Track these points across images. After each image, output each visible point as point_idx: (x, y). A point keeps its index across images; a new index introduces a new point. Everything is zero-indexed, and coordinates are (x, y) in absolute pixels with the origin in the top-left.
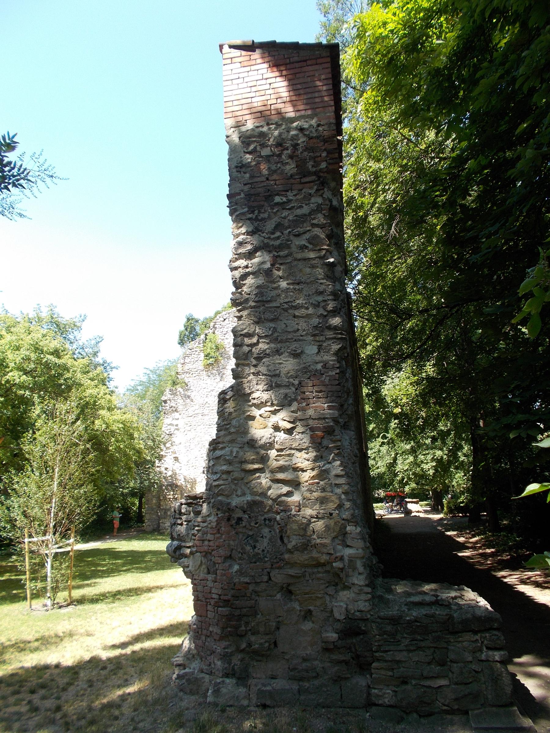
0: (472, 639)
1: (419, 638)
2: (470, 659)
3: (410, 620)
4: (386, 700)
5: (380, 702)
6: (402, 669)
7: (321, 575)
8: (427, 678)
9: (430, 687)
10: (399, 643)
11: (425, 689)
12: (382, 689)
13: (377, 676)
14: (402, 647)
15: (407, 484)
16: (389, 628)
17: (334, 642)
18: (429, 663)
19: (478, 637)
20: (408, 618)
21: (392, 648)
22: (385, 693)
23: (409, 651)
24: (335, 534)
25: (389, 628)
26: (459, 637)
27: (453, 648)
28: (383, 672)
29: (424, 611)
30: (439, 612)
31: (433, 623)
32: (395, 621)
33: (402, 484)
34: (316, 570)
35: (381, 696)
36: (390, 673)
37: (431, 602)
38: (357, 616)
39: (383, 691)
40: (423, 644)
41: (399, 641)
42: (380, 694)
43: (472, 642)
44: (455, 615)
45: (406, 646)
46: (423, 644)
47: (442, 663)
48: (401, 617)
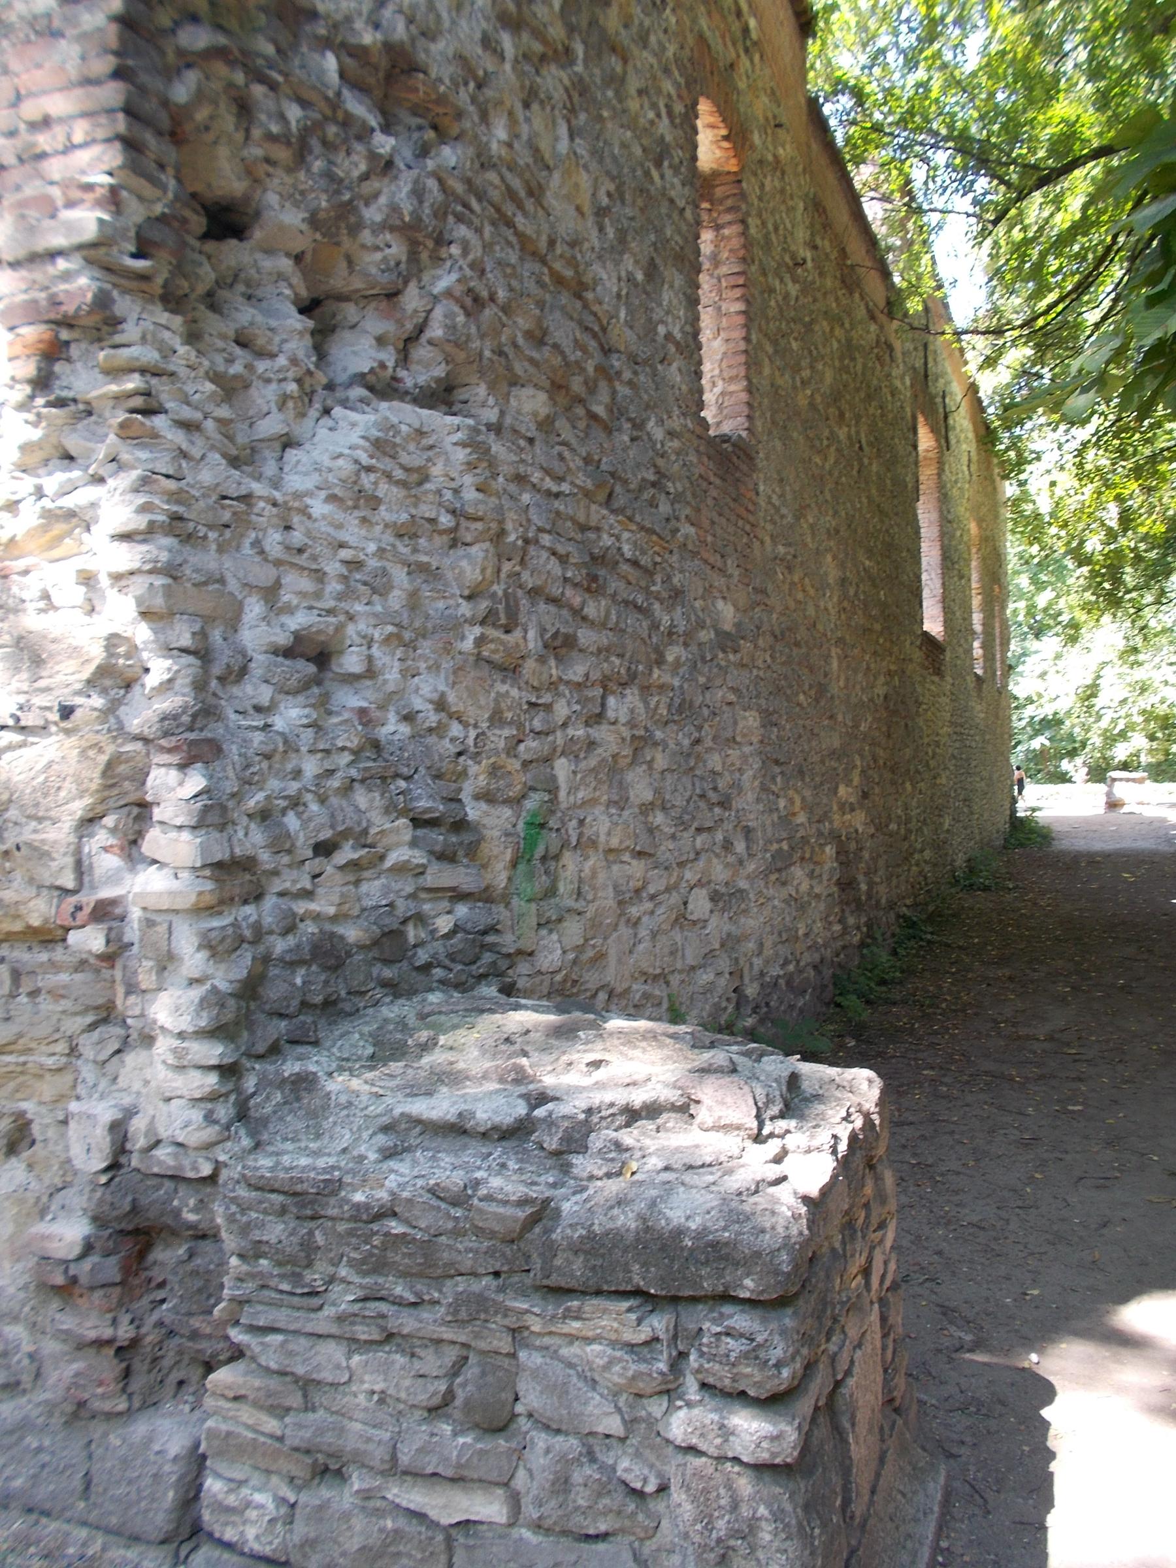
0: (629, 1336)
1: (398, 1290)
2: (614, 1425)
3: (367, 1206)
4: (251, 1532)
5: (229, 1535)
6: (321, 1413)
7: (64, 977)
8: (414, 1474)
9: (419, 1516)
10: (315, 1302)
11: (402, 1522)
12: (241, 1483)
13: (224, 1427)
14: (322, 1322)
15: (1123, 735)
16: (275, 1231)
17: (66, 1262)
18: (435, 1411)
19: (659, 1323)
20: (359, 1197)
21: (280, 1317)
22: (248, 1504)
23: (355, 1344)
24: (88, 801)
25: (275, 1231)
26: (568, 1315)
27: (537, 1359)
28: (246, 1414)
29: (448, 1168)
30: (505, 1182)
31: (457, 1233)
32: (306, 1201)
33: (1111, 739)
34: (44, 957)
35: (230, 1510)
36: (271, 1425)
37: (495, 1128)
38: (160, 1163)
39: (245, 1491)
40: (407, 1322)
41: (314, 1294)
42: (232, 1500)
43: (631, 1347)
44: (566, 1207)
45: (341, 1319)
46: (407, 1322)
47: (497, 1422)
48: (332, 1187)
